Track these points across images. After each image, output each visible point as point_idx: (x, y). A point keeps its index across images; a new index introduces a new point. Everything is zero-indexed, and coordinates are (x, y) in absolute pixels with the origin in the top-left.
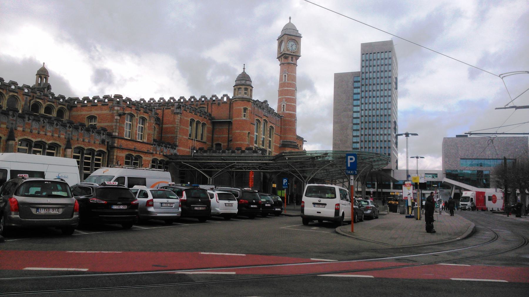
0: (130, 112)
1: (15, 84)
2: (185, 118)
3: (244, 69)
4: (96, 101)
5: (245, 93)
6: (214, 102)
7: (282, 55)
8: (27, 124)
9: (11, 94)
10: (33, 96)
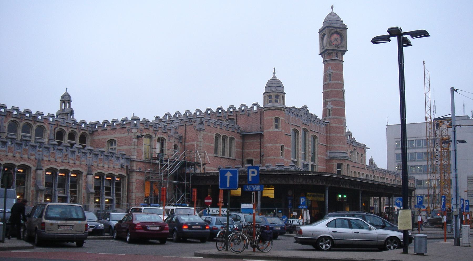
0: (147, 133)
1: (41, 114)
2: (209, 134)
3: (274, 73)
4: (106, 126)
5: (277, 101)
6: (244, 112)
7: (325, 51)
8: (52, 153)
9: (38, 124)
10: (58, 124)
